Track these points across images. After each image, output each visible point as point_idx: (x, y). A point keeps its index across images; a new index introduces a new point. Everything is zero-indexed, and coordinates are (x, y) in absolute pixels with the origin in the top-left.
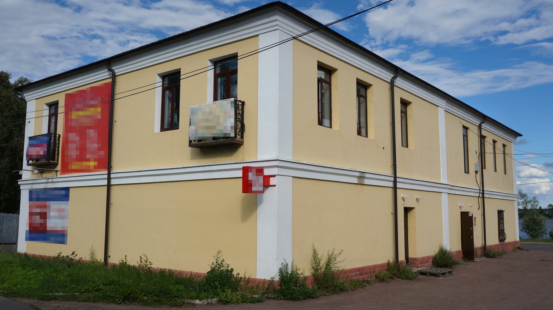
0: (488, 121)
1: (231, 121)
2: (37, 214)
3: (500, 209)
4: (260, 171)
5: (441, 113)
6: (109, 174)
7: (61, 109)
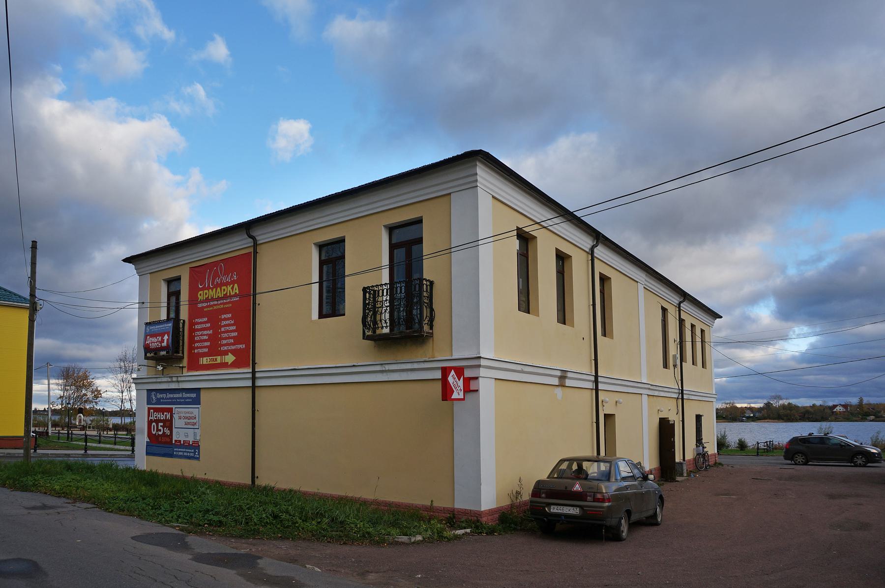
0: (689, 300)
2: (157, 421)
4: (459, 371)
6: (254, 372)
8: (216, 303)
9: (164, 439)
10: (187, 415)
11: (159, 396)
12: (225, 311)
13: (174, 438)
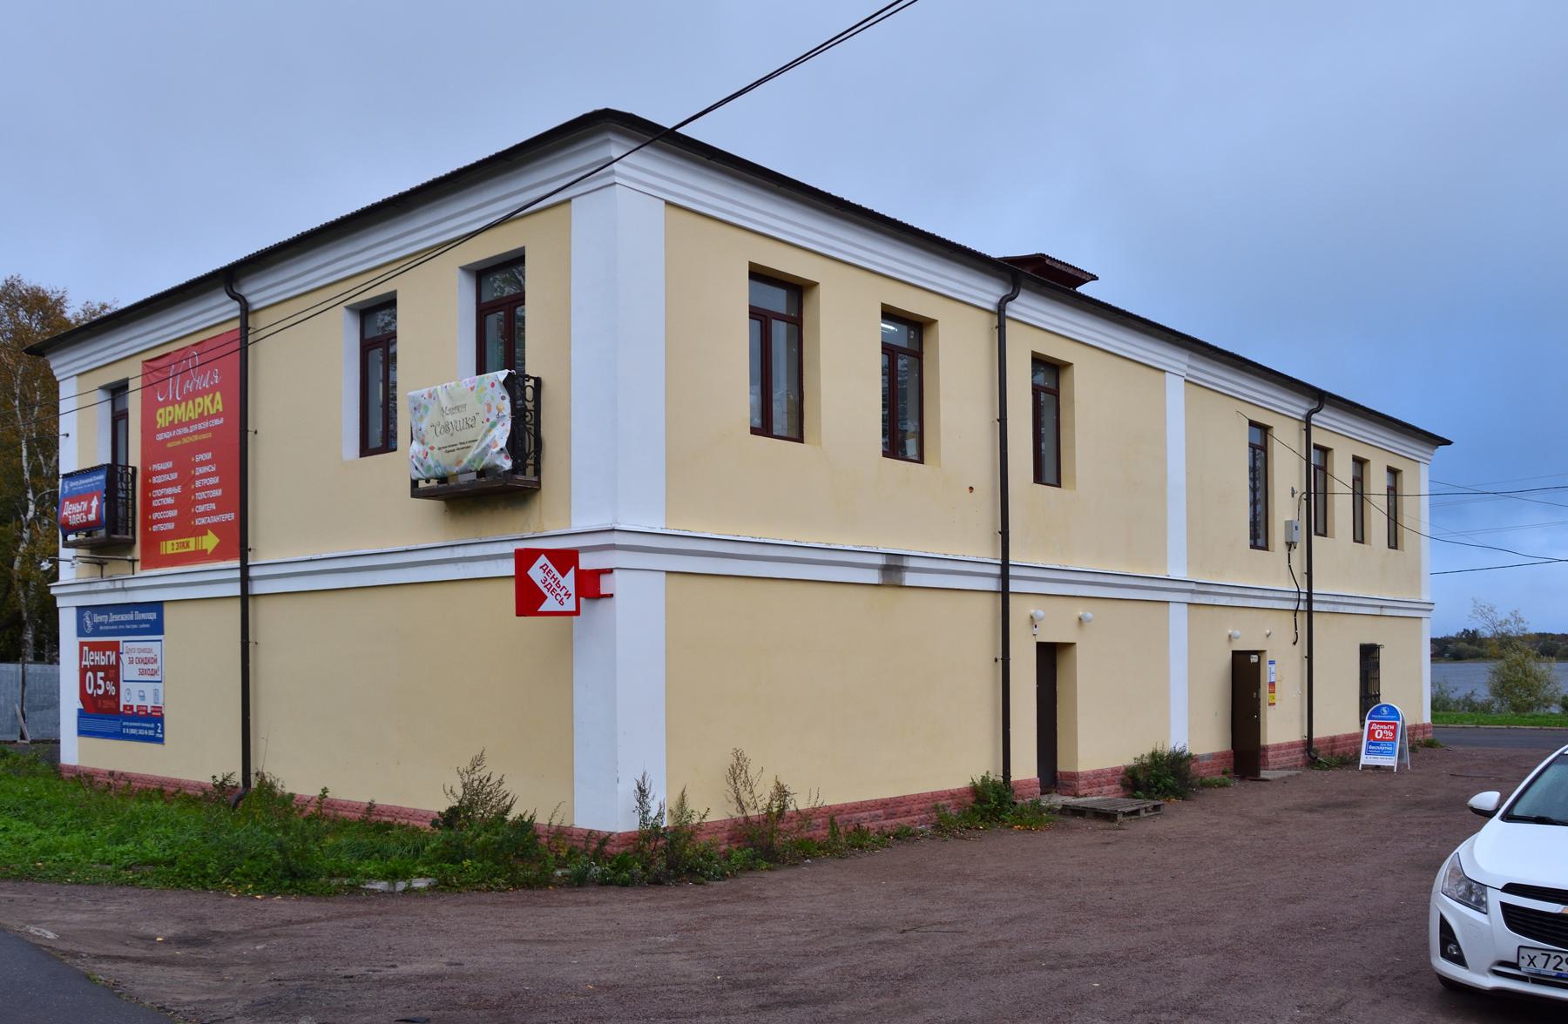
1: (501, 434)
2: (95, 669)
3: (1367, 641)
4: (564, 560)
5: (1175, 388)
6: (245, 568)
7: (134, 403)
8: (185, 430)
9: (108, 704)
10: (143, 655)
11: (98, 618)
12: (201, 447)
13: (123, 702)
